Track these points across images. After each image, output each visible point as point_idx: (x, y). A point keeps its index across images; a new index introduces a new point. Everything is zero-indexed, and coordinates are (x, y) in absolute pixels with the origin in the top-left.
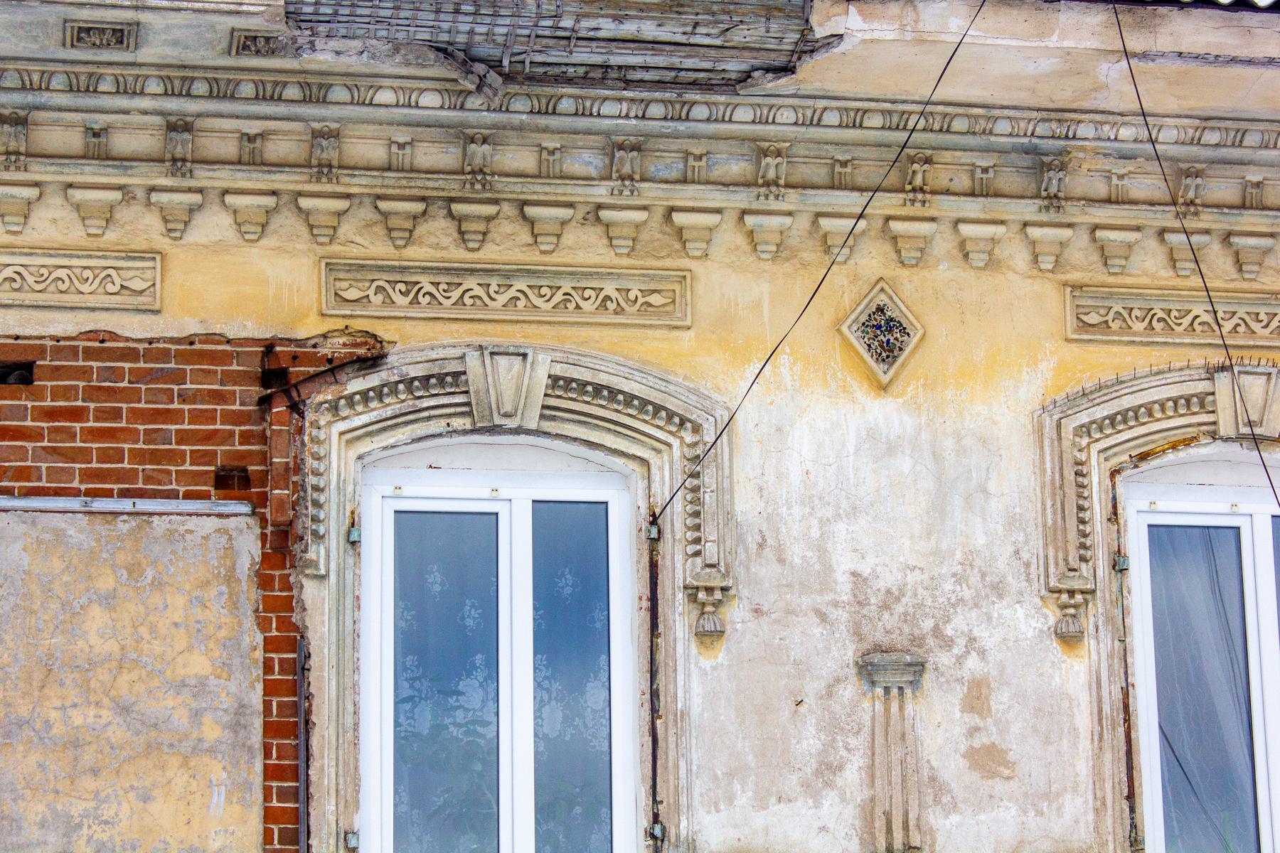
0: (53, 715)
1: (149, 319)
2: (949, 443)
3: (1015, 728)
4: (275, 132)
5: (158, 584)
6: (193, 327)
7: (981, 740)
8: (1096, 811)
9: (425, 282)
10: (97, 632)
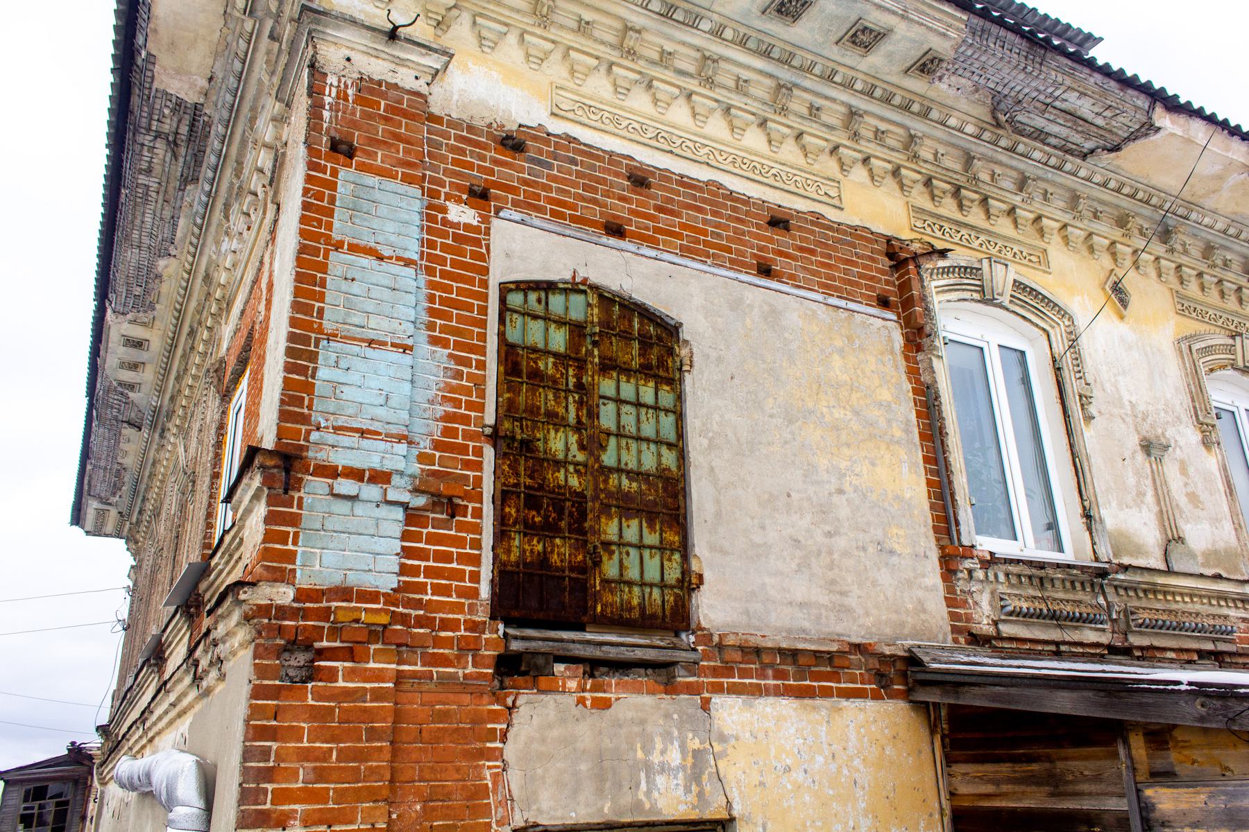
0: (825, 410)
1: (838, 212)
2: (1148, 348)
3: (1200, 485)
4: (891, 132)
5: (862, 349)
6: (856, 222)
7: (1190, 490)
8: (1236, 529)
9: (946, 226)
10: (838, 368)
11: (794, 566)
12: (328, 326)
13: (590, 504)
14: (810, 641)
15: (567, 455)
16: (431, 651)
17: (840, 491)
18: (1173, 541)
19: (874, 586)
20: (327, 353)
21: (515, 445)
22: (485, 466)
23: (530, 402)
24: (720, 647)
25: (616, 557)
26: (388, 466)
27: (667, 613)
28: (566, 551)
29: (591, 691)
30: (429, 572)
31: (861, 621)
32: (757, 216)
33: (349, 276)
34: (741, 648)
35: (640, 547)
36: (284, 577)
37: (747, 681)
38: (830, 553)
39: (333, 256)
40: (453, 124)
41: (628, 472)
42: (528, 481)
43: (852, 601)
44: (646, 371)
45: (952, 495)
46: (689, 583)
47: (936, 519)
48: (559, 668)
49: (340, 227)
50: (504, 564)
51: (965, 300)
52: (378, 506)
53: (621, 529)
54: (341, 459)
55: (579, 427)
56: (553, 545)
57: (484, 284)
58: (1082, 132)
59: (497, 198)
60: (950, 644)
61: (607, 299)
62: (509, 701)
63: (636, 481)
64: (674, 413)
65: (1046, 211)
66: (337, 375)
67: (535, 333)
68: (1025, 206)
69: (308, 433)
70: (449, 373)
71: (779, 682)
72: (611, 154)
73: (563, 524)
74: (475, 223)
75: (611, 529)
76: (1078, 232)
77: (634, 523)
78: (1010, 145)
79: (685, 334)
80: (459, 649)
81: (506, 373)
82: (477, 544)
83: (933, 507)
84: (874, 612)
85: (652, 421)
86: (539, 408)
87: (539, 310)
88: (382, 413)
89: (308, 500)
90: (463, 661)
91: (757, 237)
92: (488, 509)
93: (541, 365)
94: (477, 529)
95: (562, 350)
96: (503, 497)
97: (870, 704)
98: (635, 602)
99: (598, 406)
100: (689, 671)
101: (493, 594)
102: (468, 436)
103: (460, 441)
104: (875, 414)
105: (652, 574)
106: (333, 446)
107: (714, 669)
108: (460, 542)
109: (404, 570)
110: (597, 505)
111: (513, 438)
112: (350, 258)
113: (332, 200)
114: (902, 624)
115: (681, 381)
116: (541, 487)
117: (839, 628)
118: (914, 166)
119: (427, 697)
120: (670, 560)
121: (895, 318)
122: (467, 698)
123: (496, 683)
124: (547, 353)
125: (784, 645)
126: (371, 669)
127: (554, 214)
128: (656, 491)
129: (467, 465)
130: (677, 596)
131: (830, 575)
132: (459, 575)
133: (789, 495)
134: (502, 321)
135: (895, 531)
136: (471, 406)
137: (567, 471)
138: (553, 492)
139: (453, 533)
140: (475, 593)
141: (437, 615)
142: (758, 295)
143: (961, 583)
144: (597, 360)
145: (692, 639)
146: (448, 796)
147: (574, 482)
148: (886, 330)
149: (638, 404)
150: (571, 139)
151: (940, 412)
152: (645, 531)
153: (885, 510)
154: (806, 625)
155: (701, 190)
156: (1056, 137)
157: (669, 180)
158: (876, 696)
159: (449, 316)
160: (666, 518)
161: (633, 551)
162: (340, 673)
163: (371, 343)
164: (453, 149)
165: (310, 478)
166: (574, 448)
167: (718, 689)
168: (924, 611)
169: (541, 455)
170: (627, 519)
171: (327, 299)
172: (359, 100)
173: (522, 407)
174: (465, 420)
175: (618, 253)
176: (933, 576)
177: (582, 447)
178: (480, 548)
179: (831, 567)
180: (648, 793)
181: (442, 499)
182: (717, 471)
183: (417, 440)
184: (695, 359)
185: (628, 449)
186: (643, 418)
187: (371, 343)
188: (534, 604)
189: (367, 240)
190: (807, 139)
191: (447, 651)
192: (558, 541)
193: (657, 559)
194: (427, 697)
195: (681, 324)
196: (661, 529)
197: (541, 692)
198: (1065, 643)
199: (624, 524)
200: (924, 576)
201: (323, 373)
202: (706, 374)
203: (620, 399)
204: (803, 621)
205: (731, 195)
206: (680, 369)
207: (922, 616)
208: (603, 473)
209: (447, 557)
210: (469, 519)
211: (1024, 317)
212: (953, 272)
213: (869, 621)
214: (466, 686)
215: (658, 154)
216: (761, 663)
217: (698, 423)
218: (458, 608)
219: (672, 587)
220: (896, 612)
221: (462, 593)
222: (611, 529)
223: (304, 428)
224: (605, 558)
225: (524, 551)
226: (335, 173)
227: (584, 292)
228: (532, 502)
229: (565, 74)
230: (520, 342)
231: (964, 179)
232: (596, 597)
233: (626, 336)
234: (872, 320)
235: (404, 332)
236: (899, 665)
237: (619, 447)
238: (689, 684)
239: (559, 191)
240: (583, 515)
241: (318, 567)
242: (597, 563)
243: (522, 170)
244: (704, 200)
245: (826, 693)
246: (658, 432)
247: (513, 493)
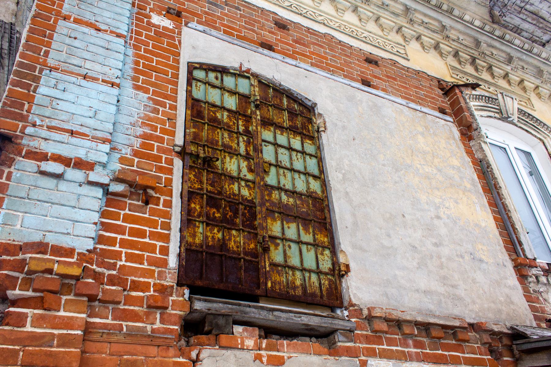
0: (419, 166)
11: (415, 264)
12: (51, 62)
13: (258, 208)
14: (438, 317)
15: (239, 174)
16: (122, 307)
17: (438, 217)
19: (474, 283)
21: (200, 160)
22: (175, 171)
23: (210, 137)
24: (370, 318)
25: (280, 248)
26: (92, 157)
27: (324, 293)
29: (266, 349)
30: (123, 243)
31: (471, 307)
33: (72, 35)
34: (387, 320)
35: (299, 242)
37: (394, 348)
39: (61, 22)
41: (286, 191)
42: (210, 188)
43: (461, 292)
44: (293, 130)
45: (513, 226)
46: (339, 272)
47: (505, 241)
48: (238, 329)
50: (190, 245)
51: (491, 117)
52: (80, 186)
53: (283, 228)
54: (50, 148)
55: (247, 157)
56: (230, 235)
58: (542, 28)
59: (186, 17)
60: (534, 325)
61: (265, 84)
62: (194, 355)
63: (293, 197)
64: (316, 157)
65: (526, 77)
67: (214, 96)
68: (513, 73)
69: (24, 127)
70: (148, 109)
71: (419, 350)
73: (238, 221)
74: (171, 27)
76: (545, 91)
77: (293, 226)
78: (501, 34)
79: (319, 109)
80: (149, 307)
81: (192, 115)
82: (167, 226)
83: (501, 234)
84: (478, 301)
85: (301, 161)
86: (218, 141)
88: (91, 122)
89: (16, 175)
90: (151, 317)
92: (176, 201)
93: (219, 115)
94: (168, 215)
95: (234, 108)
96: (189, 196)
98: (298, 283)
99: (261, 145)
100: (347, 337)
101: (180, 266)
103: (155, 152)
104: (451, 172)
105: (310, 261)
106: (46, 139)
107: (367, 337)
108: (154, 224)
109: (100, 239)
110: (264, 209)
111: (198, 156)
112: (74, 26)
115: (319, 138)
116: (220, 193)
118: (447, 43)
119: (116, 348)
120: (322, 254)
121: (452, 120)
122: (153, 350)
123: (183, 342)
124: (223, 108)
125: (419, 319)
126: (60, 317)
127: (225, 32)
128: (308, 206)
129: (160, 169)
130: (330, 281)
132: (151, 248)
133: (404, 216)
134: (189, 83)
135: (480, 247)
137: (239, 184)
138: (230, 197)
139: (146, 216)
140: (165, 263)
141: (130, 278)
142: (364, 97)
143: (532, 285)
144: (259, 117)
145: (346, 313)
147: (245, 192)
148: (448, 128)
149: (290, 149)
151: (493, 174)
152: (302, 232)
153: (471, 233)
154: (432, 307)
156: (527, 32)
160: (316, 224)
161: (293, 245)
162: (29, 319)
165: (21, 159)
166: (245, 171)
167: (372, 353)
168: (512, 303)
169: (220, 172)
170: (287, 223)
171: (53, 47)
173: (205, 138)
174: (160, 140)
175: (270, 59)
176: (513, 280)
177: (250, 170)
178: (169, 229)
179: (441, 266)
181: (135, 190)
182: (351, 195)
183: (120, 148)
184: (328, 125)
185: (285, 176)
186: (294, 157)
188: (215, 277)
189: (88, 17)
190: (382, 20)
191: (136, 308)
192: (234, 232)
193: (312, 253)
194: (116, 348)
195: (316, 104)
196: (313, 232)
197: (222, 347)
199: (286, 226)
200: (506, 279)
201: (42, 90)
202: (336, 135)
206: (318, 131)
207: (512, 307)
208: (267, 189)
209: (142, 234)
210: (161, 207)
211: (527, 131)
212: (482, 99)
213: (476, 308)
214: (152, 339)
216: (403, 334)
217: (334, 163)
218: (150, 273)
219: (326, 274)
220: (493, 302)
221: (153, 262)
223: (21, 124)
224: (272, 248)
225: (207, 237)
227: (248, 78)
228: (213, 201)
230: (203, 99)
231: (476, 53)
232: (267, 276)
233: (279, 108)
234: (438, 120)
235: (113, 74)
236: (506, 341)
237: (278, 174)
238: (348, 349)
240: (254, 216)
241: (18, 227)
242: (266, 250)
246: (305, 168)
247: (198, 194)
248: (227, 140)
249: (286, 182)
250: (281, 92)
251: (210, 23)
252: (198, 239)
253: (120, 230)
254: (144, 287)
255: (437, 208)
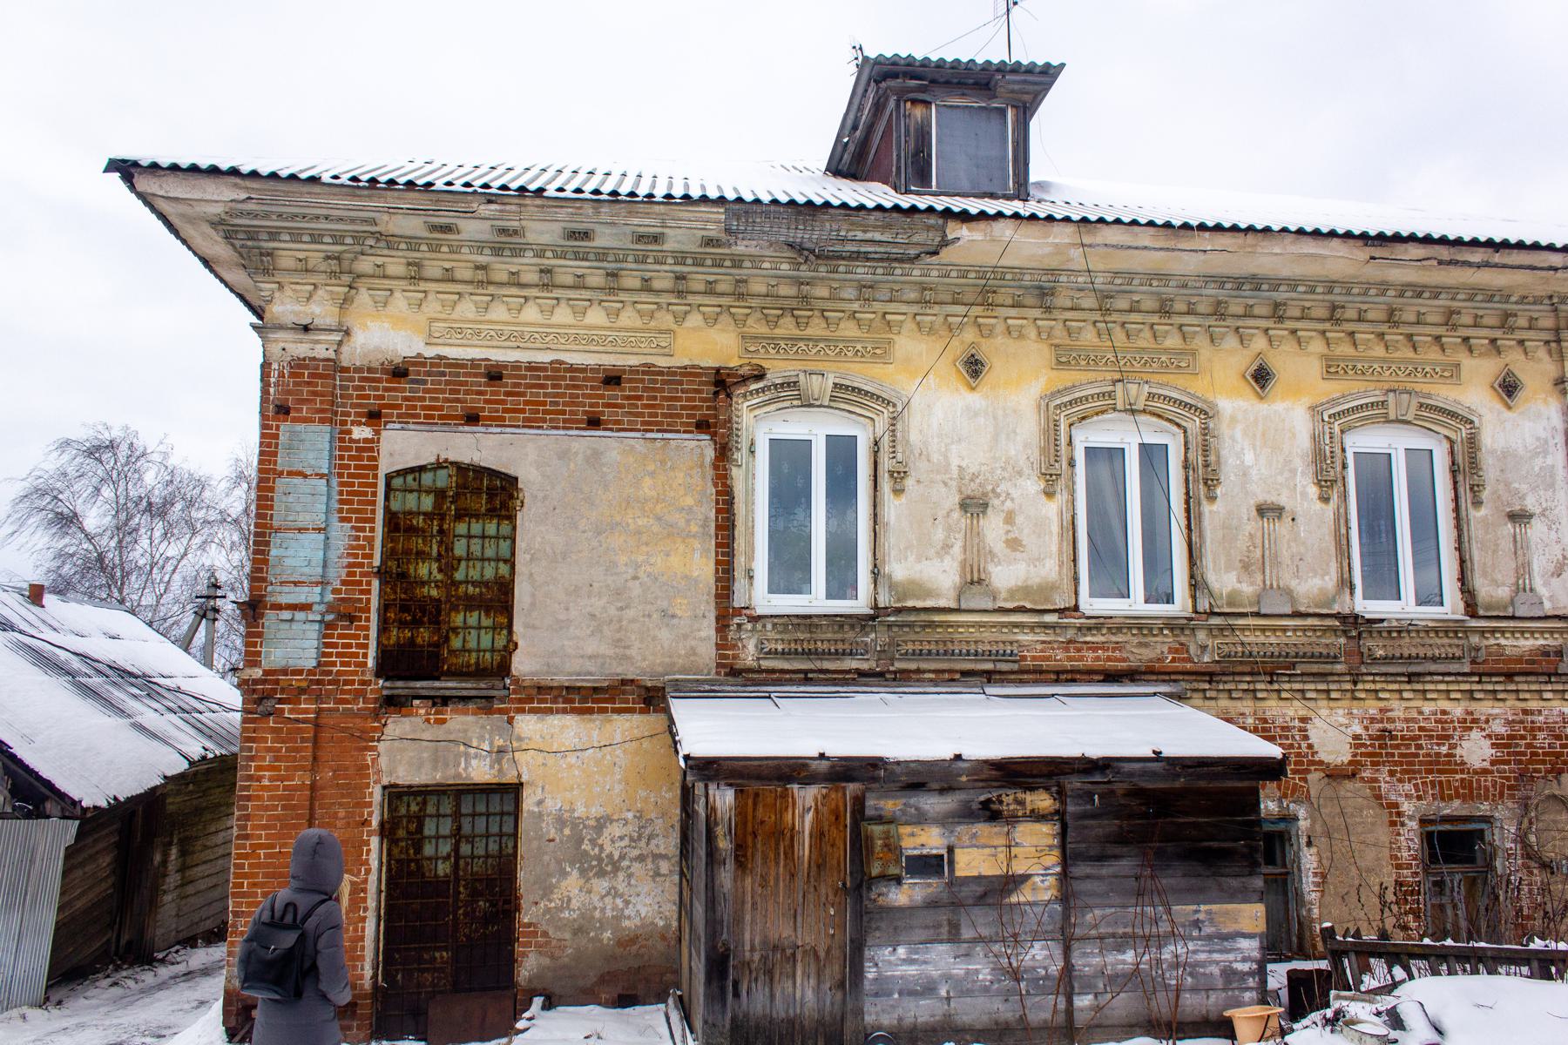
2: (1000, 413)
6: (687, 362)
12: (275, 524)
18: (974, 580)
20: (275, 540)
21: (394, 576)
26: (310, 600)
28: (426, 635)
30: (339, 655)
32: (593, 379)
36: (256, 664)
38: (620, 621)
40: (358, 370)
43: (633, 652)
44: (492, 513)
46: (511, 647)
48: (416, 702)
49: (282, 462)
54: (284, 599)
57: (375, 476)
59: (387, 415)
61: (461, 469)
66: (280, 552)
67: (411, 501)
72: (472, 360)
75: (458, 619)
77: (476, 614)
87: (415, 485)
88: (306, 570)
91: (590, 396)
92: (374, 616)
94: (367, 628)
96: (385, 608)
97: (636, 718)
102: (363, 574)
108: (356, 637)
113: (277, 445)
114: (673, 664)
117: (619, 670)
122: (358, 721)
129: (362, 592)
131: (618, 636)
132: (356, 655)
134: (387, 498)
136: (365, 556)
140: (365, 664)
142: (583, 442)
146: (346, 769)
147: (434, 593)
150: (440, 357)
155: (545, 369)
157: (519, 368)
158: (642, 711)
159: (351, 506)
163: (299, 530)
164: (356, 388)
166: (435, 572)
167: (522, 711)
168: (695, 654)
172: (292, 375)
174: (361, 565)
176: (708, 630)
177: (440, 570)
180: (465, 769)
181: (345, 614)
187: (299, 530)
189: (297, 467)
193: (490, 635)
198: (812, 671)
201: (274, 552)
203: (468, 537)
204: (590, 666)
205: (572, 369)
215: (509, 351)
218: (355, 673)
221: (357, 665)
222: (458, 619)
226: (278, 428)
229: (440, 308)
232: (444, 661)
239: (432, 399)
240: (439, 612)
242: (447, 639)
243: (404, 390)
244: (547, 378)
245: (603, 711)
248: (421, 546)
249: (475, 574)
250: (480, 471)
251: (408, 417)
252: (393, 640)
253: (335, 645)
254: (352, 682)
255: (638, 566)
